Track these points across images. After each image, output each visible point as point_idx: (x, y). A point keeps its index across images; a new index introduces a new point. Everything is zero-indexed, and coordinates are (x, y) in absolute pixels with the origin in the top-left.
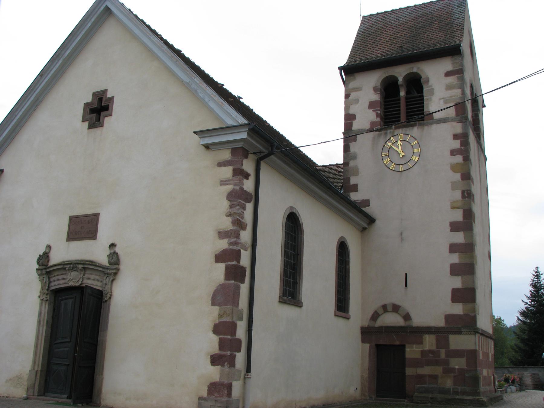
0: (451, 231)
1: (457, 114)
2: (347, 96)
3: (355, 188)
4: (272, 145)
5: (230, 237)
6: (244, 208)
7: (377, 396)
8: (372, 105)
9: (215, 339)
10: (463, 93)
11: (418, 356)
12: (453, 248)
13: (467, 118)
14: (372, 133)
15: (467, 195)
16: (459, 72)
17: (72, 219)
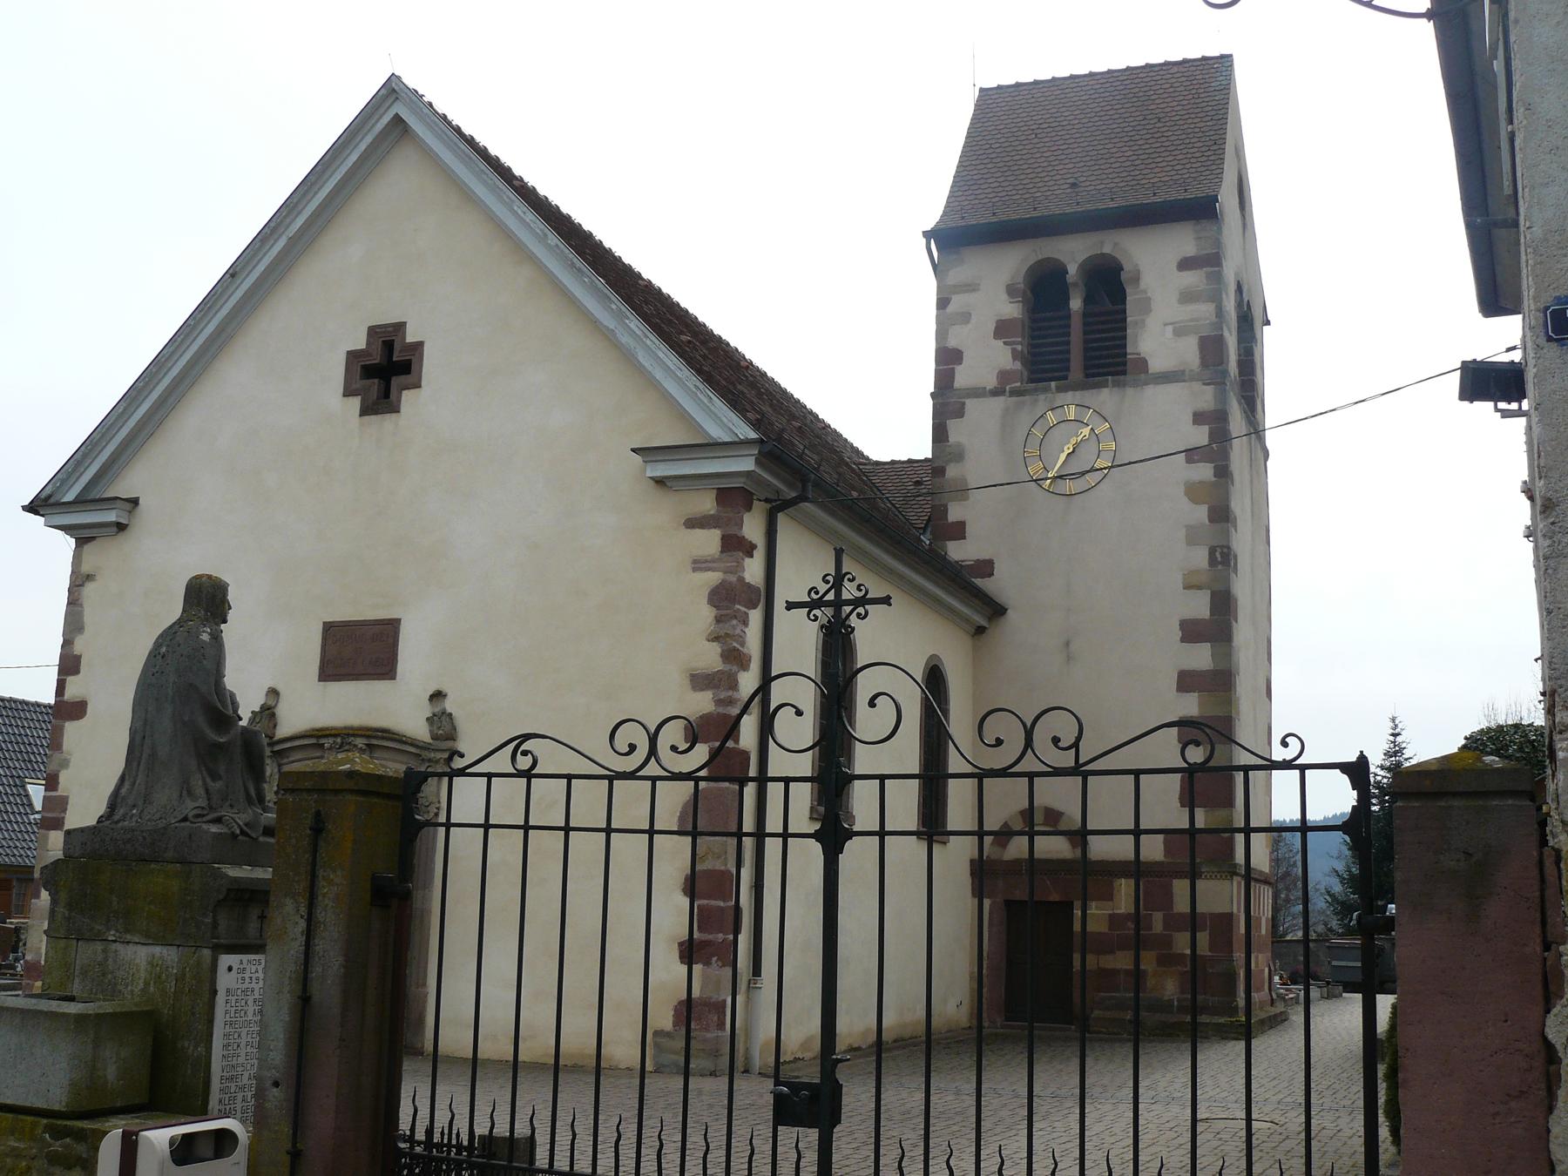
0: (1183, 640)
1: (1204, 363)
2: (942, 303)
3: (958, 531)
4: (804, 481)
5: (716, 687)
6: (745, 623)
7: (1007, 1019)
8: (1003, 329)
10: (1220, 312)
12: (1187, 681)
13: (1225, 373)
14: (1002, 398)
15: (1222, 558)
16: (1210, 261)
17: (329, 628)
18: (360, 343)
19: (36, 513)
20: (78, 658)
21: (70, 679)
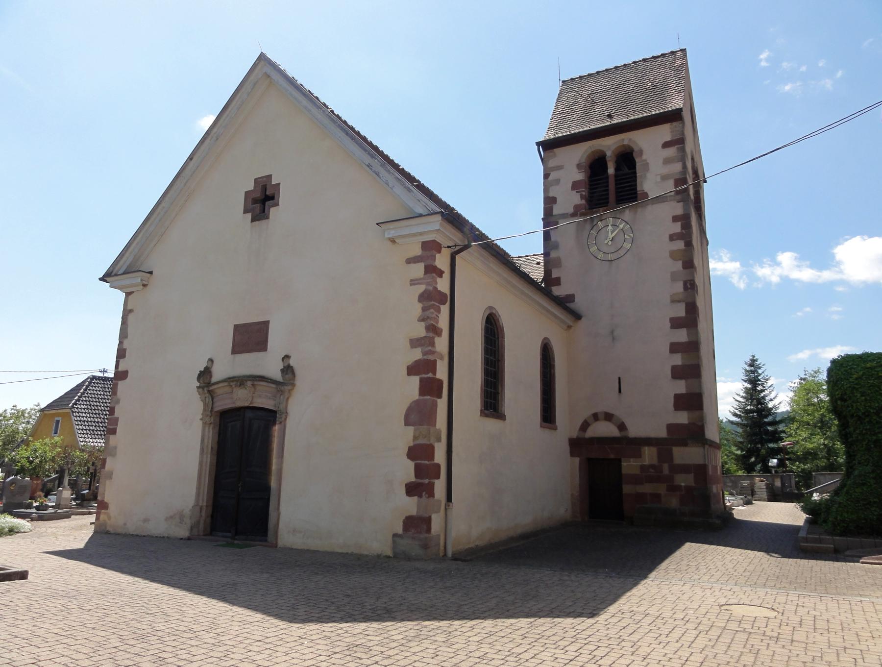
2: (546, 176)
5: (421, 345)
6: (439, 311)
8: (575, 186)
9: (411, 465)
10: (685, 167)
11: (637, 472)
12: (675, 348)
15: (690, 286)
16: (679, 142)
17: (237, 328)
18: (251, 187)
19: (106, 281)
20: (125, 350)
21: (121, 361)
